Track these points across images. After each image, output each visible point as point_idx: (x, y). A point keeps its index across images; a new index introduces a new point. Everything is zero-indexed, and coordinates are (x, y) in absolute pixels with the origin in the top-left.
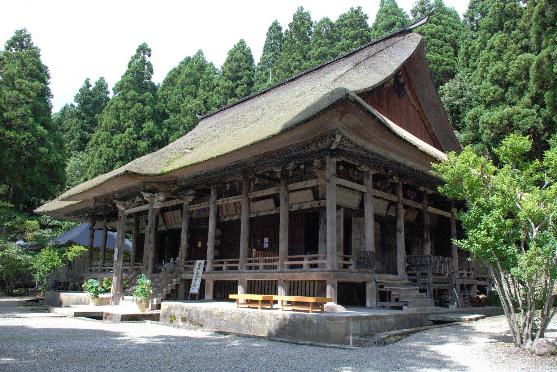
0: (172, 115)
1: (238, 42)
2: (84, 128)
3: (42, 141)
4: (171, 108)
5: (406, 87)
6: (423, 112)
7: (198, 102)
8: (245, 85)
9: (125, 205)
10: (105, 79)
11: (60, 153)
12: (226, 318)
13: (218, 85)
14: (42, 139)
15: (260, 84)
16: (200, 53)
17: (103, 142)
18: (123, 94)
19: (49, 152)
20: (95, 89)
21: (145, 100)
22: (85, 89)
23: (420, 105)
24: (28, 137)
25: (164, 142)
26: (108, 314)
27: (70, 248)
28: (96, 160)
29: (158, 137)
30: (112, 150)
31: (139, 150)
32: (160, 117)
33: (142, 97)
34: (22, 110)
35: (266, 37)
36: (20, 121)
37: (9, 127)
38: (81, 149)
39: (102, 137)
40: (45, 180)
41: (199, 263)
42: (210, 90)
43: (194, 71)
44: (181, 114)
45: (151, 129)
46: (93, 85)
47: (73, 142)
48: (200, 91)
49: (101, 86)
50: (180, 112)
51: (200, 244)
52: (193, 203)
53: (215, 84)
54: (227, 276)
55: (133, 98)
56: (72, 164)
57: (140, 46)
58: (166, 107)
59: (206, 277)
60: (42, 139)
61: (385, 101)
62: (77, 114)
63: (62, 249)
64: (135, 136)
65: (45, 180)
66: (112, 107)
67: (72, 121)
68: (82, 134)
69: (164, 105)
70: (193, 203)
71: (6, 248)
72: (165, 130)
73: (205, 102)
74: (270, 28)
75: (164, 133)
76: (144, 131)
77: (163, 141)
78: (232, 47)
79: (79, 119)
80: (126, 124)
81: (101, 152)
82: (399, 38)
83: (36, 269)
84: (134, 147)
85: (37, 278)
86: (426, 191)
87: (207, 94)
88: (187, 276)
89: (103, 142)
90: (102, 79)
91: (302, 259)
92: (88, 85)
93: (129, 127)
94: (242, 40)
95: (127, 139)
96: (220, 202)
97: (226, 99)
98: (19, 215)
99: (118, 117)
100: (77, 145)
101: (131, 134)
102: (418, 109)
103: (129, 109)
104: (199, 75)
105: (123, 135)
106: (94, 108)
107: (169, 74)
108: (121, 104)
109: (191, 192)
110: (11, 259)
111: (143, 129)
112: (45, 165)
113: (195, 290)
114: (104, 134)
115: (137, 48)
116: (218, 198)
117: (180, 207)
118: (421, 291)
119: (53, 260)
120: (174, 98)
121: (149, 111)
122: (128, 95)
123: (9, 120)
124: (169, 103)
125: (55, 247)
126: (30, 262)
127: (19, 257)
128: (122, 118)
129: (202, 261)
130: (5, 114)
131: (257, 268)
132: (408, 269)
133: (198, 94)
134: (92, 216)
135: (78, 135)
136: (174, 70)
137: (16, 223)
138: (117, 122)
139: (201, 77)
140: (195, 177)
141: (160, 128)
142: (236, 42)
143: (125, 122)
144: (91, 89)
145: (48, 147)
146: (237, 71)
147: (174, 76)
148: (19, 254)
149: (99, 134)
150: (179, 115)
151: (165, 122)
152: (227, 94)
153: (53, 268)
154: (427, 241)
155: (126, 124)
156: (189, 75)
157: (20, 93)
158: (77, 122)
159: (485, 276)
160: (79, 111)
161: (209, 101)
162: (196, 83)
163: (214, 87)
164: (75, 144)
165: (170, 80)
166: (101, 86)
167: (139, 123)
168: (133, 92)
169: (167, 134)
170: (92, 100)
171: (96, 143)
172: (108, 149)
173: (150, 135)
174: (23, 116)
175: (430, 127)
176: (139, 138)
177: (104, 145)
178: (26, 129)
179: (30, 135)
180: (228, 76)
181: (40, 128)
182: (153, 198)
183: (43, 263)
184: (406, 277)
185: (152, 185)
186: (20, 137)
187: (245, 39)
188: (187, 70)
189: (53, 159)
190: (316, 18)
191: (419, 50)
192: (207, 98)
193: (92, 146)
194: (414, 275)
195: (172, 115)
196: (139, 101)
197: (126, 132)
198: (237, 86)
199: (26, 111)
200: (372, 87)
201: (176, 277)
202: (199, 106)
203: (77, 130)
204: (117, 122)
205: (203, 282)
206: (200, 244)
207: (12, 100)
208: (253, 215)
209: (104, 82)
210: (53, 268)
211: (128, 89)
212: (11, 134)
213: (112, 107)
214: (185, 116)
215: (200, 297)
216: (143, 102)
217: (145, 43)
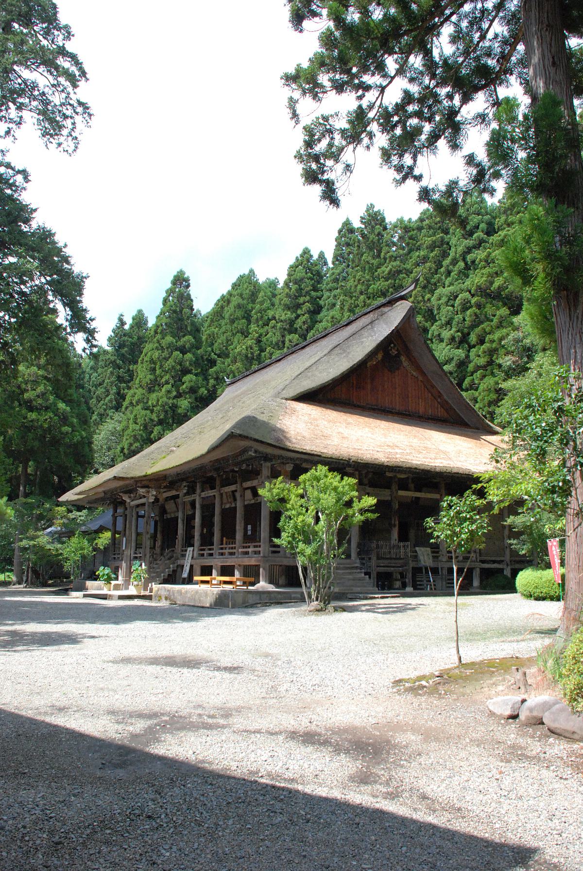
0: (219, 360)
1: (300, 252)
2: (120, 379)
3: (64, 420)
4: (218, 352)
5: (403, 358)
6: (428, 380)
7: (249, 343)
8: (307, 315)
9: (130, 497)
10: (144, 312)
11: (84, 430)
12: (189, 595)
13: (274, 318)
14: (64, 418)
15: (328, 310)
16: (252, 271)
17: (138, 402)
18: (158, 342)
19: (73, 431)
20: (132, 327)
21: (184, 347)
22: (118, 328)
23: (423, 373)
24: (50, 418)
25: (212, 397)
26: (110, 596)
27: (101, 535)
28: (132, 426)
29: (203, 391)
30: (148, 412)
31: (180, 411)
32: (205, 364)
33: (180, 344)
34: (41, 389)
35: (335, 243)
36: (40, 401)
37: (31, 409)
38: (117, 407)
39: (136, 398)
40: (69, 462)
41: (190, 549)
42: (265, 325)
43: (247, 295)
44: (229, 360)
45: (192, 384)
46: (129, 321)
47: (109, 398)
48: (253, 327)
49: (140, 320)
50: (227, 356)
51: (205, 530)
52: (185, 495)
53: (270, 317)
54: (207, 562)
55: (170, 345)
56: (101, 436)
57: (175, 277)
58: (212, 351)
59: (194, 562)
60: (64, 418)
61: (369, 381)
62: (111, 362)
63: (93, 535)
64: (174, 393)
65: (69, 462)
66: (146, 359)
67: (106, 371)
68: (119, 388)
69: (210, 349)
70: (185, 495)
71: (38, 537)
72: (212, 382)
73: (259, 341)
74: (340, 231)
75: (210, 385)
76: (184, 387)
77: (210, 395)
78: (292, 261)
79: (114, 369)
80: (163, 380)
81: (136, 416)
82: (386, 309)
83: (67, 558)
84: (174, 407)
85: (67, 566)
86: (395, 476)
87: (261, 331)
88: (180, 562)
89: (138, 402)
90: (140, 312)
91: (249, 547)
92: (122, 323)
93: (167, 383)
94: (307, 249)
95: (165, 399)
96: (203, 495)
97: (283, 336)
98: (46, 502)
99: (154, 370)
100: (114, 402)
101: (169, 392)
102: (420, 378)
103: (166, 359)
104: (250, 306)
105: (160, 394)
106: (132, 351)
107: (216, 304)
108: (156, 354)
109: (185, 484)
110: (42, 548)
111: (183, 384)
112: (70, 446)
113: (185, 575)
114: (140, 391)
115: (172, 278)
116: (203, 491)
117: (176, 497)
118: (366, 574)
119: (82, 549)
120: (222, 339)
121: (191, 361)
122: (164, 343)
123: (30, 401)
124: (216, 345)
125: (85, 533)
126: (61, 551)
127: (48, 547)
128: (158, 372)
129: (191, 549)
130: (26, 396)
131: (247, 553)
132: (359, 554)
133: (250, 331)
134: (113, 503)
135: (114, 390)
136: (223, 297)
137: (45, 509)
138: (152, 377)
139: (253, 309)
140: (178, 474)
141: (206, 379)
142: (299, 252)
143: (162, 377)
144: (127, 327)
145: (72, 425)
146: (296, 297)
147: (222, 307)
148: (49, 543)
149: (134, 393)
150: (228, 361)
151: (212, 371)
152: (285, 329)
153: (83, 557)
154: (395, 526)
155: (163, 380)
156: (239, 306)
157: (39, 369)
158: (112, 373)
159: (502, 559)
160: (113, 358)
161: (264, 339)
162: (248, 317)
163: (270, 320)
164: (111, 401)
165: (218, 312)
166: (140, 320)
167: (178, 380)
168: (169, 339)
169: (214, 386)
170: (130, 341)
171: (131, 403)
172: (144, 412)
173: (193, 390)
174: (43, 395)
175: (440, 396)
176: (179, 395)
177: (139, 407)
178: (47, 408)
179: (52, 415)
180: (285, 305)
181: (62, 405)
182: (148, 492)
183: (72, 550)
184: (358, 561)
185: (143, 483)
186: (42, 418)
187: (309, 248)
188: (235, 301)
189: (77, 439)
190: (391, 218)
191: (409, 318)
192: (261, 335)
193: (127, 408)
194: (363, 559)
195: (219, 360)
196: (176, 350)
197: (164, 389)
198: (298, 317)
199: (45, 389)
200: (332, 379)
201: (174, 563)
202: (251, 348)
203: (112, 383)
204: (152, 377)
205: (192, 566)
206: (205, 530)
207: (32, 378)
208: (246, 503)
209: (143, 315)
210: (83, 557)
211: (164, 334)
212: (33, 416)
213: (146, 359)
214: (234, 361)
215: (189, 581)
216: (183, 351)
217: (181, 271)
